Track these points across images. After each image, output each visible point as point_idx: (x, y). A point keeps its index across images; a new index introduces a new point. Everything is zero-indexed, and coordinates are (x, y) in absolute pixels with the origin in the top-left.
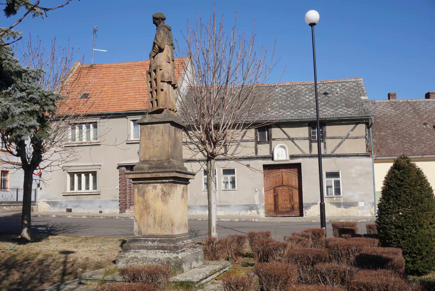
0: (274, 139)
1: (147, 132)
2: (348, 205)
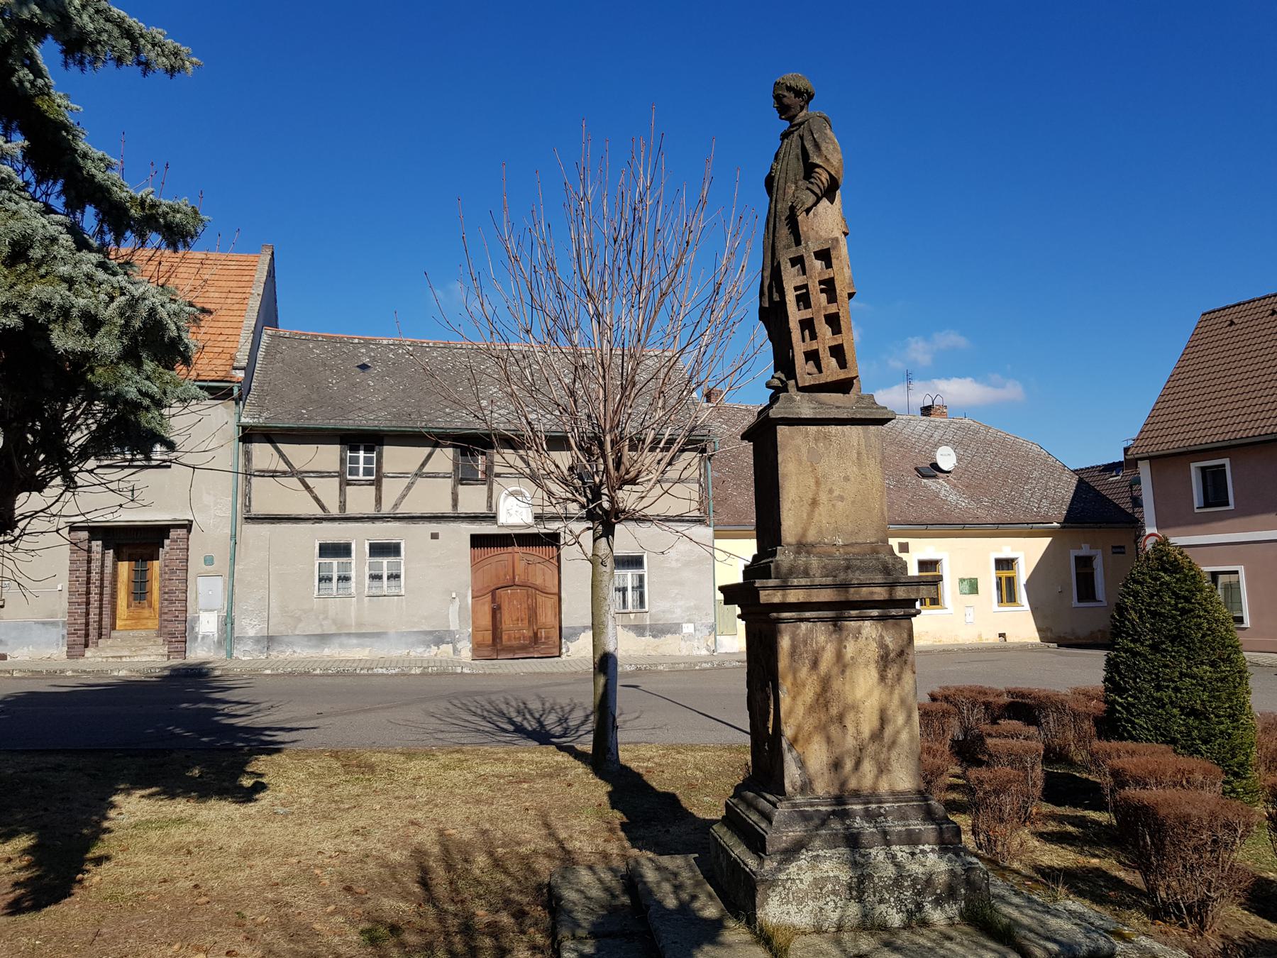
0: (498, 475)
1: (804, 450)
2: (659, 630)
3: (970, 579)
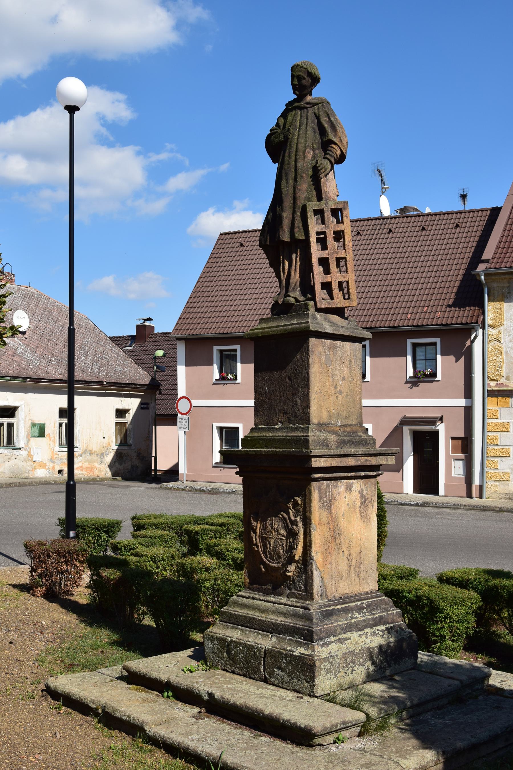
1: (323, 356)
3: (40, 424)
